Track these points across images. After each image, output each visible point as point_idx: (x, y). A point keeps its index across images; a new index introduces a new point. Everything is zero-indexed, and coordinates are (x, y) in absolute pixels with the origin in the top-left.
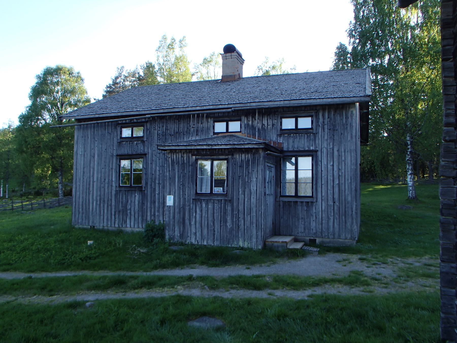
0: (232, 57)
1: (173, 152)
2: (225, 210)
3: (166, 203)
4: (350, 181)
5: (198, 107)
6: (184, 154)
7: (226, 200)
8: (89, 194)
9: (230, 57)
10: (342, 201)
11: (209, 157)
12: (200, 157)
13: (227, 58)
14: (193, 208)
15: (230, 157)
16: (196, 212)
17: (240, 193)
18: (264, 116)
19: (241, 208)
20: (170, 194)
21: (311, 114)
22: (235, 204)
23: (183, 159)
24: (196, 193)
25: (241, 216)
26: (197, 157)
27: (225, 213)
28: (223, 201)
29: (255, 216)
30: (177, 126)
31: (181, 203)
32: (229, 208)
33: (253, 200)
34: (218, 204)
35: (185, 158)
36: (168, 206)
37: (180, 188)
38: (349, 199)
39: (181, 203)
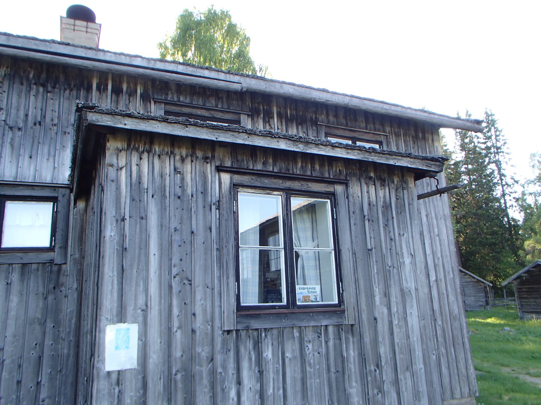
0: (89, 30)
1: (137, 150)
2: (342, 360)
3: (103, 361)
4: (452, 276)
5: (139, 59)
6: (183, 160)
7: (339, 327)
8: (19, 374)
9: (85, 29)
10: (446, 315)
11: (279, 183)
12: (245, 179)
13: (76, 28)
14: (224, 367)
15: (339, 189)
16: (239, 383)
17: (377, 299)
18: (290, 125)
19: (384, 350)
20: (121, 318)
21: (379, 139)
22: (367, 339)
23: (183, 179)
24: (240, 308)
25: (388, 375)
26: (237, 178)
27: (342, 371)
28: (330, 329)
29: (423, 370)
30: (39, 105)
31: (177, 353)
32: (352, 354)
33: (414, 321)
34: (316, 343)
35: (188, 178)
36: (109, 373)
37: (170, 287)
38: (456, 311)
39: (177, 353)
